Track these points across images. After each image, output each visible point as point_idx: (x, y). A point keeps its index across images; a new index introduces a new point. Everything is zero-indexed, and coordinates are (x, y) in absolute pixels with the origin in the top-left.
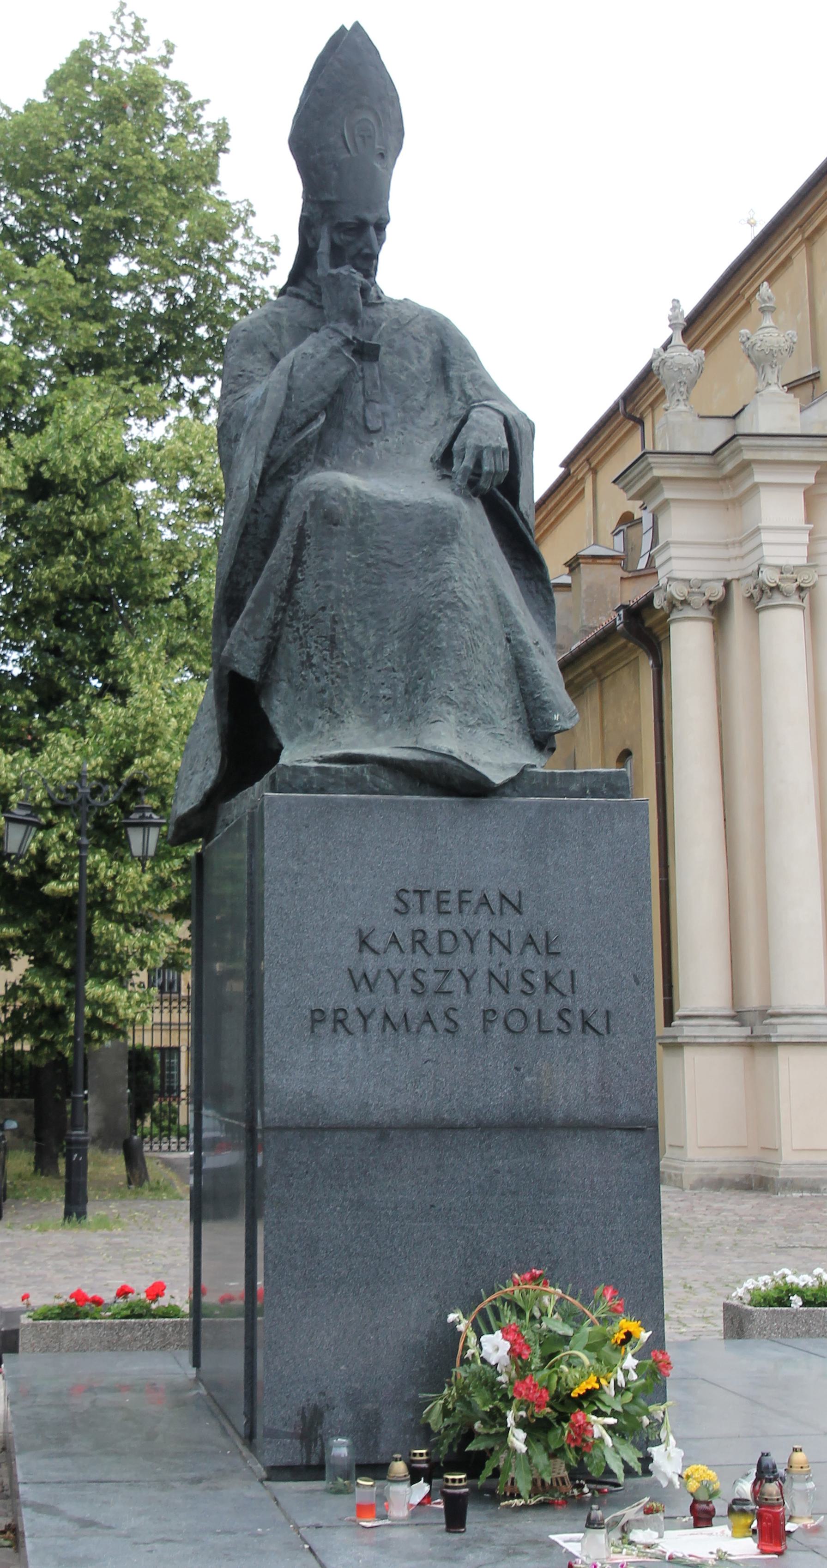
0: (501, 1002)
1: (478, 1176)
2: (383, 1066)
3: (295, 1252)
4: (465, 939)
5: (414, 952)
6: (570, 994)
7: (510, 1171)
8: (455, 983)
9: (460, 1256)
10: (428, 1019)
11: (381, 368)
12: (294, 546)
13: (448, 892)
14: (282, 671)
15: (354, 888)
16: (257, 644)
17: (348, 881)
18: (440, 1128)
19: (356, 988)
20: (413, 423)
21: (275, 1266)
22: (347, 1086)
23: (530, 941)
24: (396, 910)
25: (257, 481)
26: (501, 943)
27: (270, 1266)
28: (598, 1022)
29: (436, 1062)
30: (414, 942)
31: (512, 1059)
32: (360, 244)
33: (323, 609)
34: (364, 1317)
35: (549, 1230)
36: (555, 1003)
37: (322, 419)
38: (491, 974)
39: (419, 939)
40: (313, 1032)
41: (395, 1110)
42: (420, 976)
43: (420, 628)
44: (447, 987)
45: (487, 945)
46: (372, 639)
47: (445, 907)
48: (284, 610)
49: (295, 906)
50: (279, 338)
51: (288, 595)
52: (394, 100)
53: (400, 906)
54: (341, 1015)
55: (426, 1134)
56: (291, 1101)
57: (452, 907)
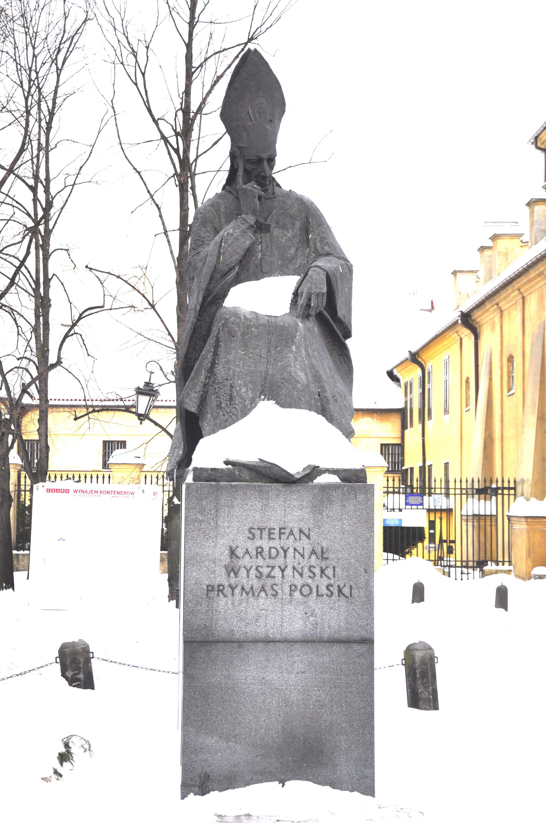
0: (298, 581)
1: (286, 664)
2: (241, 612)
3: (198, 699)
4: (282, 551)
5: (257, 557)
6: (332, 578)
7: (301, 662)
8: (277, 572)
9: (276, 702)
10: (263, 589)
11: (271, 236)
12: (213, 346)
13: (274, 529)
14: (209, 408)
15: (228, 527)
16: (196, 395)
17: (226, 524)
18: (267, 641)
19: (229, 575)
20: (287, 267)
21: (188, 706)
22: (224, 622)
23: (313, 552)
24: (249, 538)
25: (198, 308)
26: (299, 553)
27: (186, 706)
28: (346, 591)
29: (267, 610)
30: (257, 553)
31: (304, 609)
32: (260, 170)
33: (227, 380)
34: (230, 731)
35: (319, 690)
36: (325, 581)
37: (237, 269)
38: (294, 568)
39: (259, 552)
40: (208, 596)
41: (246, 633)
42: (260, 569)
43: (273, 391)
44: (273, 574)
45: (293, 554)
46: (250, 395)
47: (272, 536)
48: (209, 378)
49: (200, 536)
50: (220, 219)
51: (211, 370)
52: (280, 87)
53: (251, 536)
54: (221, 588)
55: (261, 645)
56: (196, 629)
57: (276, 536)
